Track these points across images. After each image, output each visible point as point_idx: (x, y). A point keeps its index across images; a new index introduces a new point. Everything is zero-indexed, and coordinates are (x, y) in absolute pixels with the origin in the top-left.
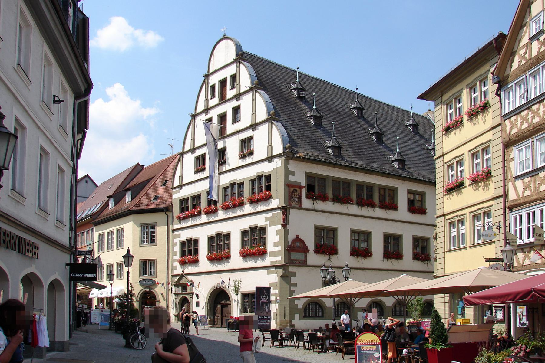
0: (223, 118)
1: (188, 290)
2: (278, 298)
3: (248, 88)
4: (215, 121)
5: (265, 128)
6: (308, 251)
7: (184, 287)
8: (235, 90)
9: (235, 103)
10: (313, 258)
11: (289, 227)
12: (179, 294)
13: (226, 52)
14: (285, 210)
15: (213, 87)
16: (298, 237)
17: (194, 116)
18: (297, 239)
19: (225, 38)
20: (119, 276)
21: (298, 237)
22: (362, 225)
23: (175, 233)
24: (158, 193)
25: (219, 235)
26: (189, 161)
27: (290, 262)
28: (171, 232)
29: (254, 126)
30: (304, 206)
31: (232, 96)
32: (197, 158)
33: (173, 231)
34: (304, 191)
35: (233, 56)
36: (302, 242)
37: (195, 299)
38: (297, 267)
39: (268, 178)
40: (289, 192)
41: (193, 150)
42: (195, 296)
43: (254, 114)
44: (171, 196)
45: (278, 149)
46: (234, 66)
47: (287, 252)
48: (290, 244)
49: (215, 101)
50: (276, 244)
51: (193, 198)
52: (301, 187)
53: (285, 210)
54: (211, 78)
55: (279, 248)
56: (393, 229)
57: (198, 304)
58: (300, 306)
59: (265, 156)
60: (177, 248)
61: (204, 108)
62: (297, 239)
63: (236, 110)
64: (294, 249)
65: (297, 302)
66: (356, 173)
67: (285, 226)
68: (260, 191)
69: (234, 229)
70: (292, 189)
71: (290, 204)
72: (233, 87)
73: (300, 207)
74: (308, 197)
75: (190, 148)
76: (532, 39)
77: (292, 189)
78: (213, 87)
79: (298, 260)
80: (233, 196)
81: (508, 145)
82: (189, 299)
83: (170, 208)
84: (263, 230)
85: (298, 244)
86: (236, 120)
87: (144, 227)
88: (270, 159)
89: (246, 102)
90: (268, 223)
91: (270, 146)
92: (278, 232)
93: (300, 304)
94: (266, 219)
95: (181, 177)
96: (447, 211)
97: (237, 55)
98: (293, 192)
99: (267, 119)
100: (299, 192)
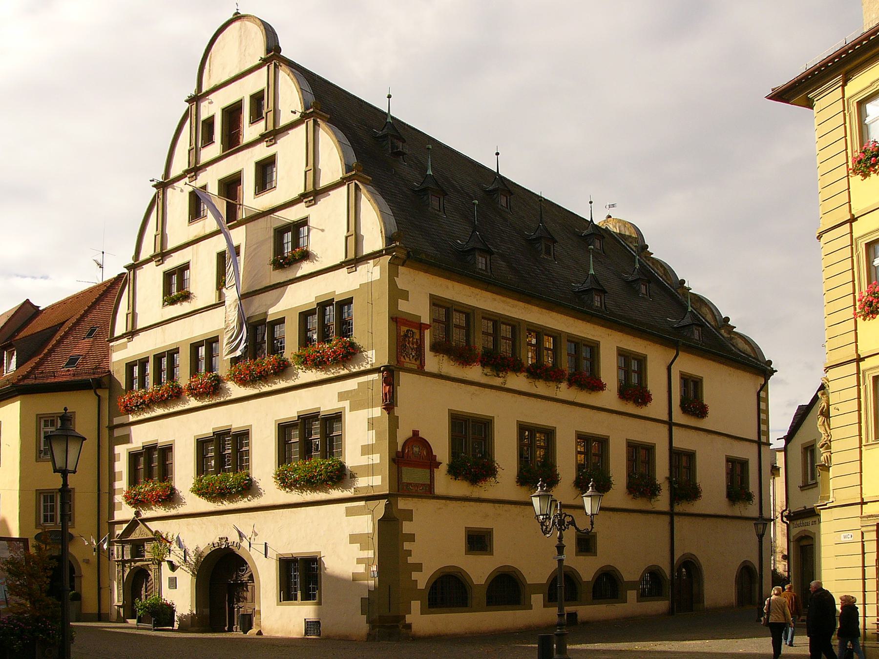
0: (230, 186)
2: (374, 568)
3: (297, 116)
7: (138, 548)
8: (263, 123)
9: (262, 152)
10: (443, 482)
11: (397, 411)
12: (128, 561)
13: (242, 49)
14: (390, 375)
15: (209, 123)
16: (416, 433)
17: (163, 186)
18: (416, 438)
19: (237, 17)
21: (416, 433)
22: (539, 414)
23: (118, 433)
24: (75, 352)
25: (220, 436)
26: (150, 281)
27: (399, 489)
28: (105, 432)
30: (427, 368)
31: (256, 136)
32: (168, 276)
33: (112, 428)
35: (259, 52)
36: (425, 444)
38: (415, 500)
40: (398, 335)
41: (162, 255)
44: (106, 356)
45: (373, 238)
47: (395, 467)
48: (400, 449)
50: (367, 450)
51: (158, 358)
52: (422, 327)
54: (204, 105)
55: (376, 458)
56: (596, 424)
57: (173, 583)
58: (422, 585)
59: (341, 258)
60: (122, 466)
61: (186, 167)
62: (416, 438)
63: (265, 170)
64: (408, 457)
65: (415, 575)
66: (527, 305)
67: (390, 405)
68: (324, 337)
70: (404, 329)
72: (257, 116)
73: (420, 371)
74: (436, 348)
75: (152, 253)
77: (404, 329)
78: (209, 123)
79: (417, 485)
83: (105, 380)
84: (336, 418)
85: (416, 449)
88: (354, 262)
90: (346, 404)
92: (372, 423)
93: (422, 579)
95: (133, 315)
97: (268, 51)
98: (406, 336)
99: (343, 179)
100: (417, 336)
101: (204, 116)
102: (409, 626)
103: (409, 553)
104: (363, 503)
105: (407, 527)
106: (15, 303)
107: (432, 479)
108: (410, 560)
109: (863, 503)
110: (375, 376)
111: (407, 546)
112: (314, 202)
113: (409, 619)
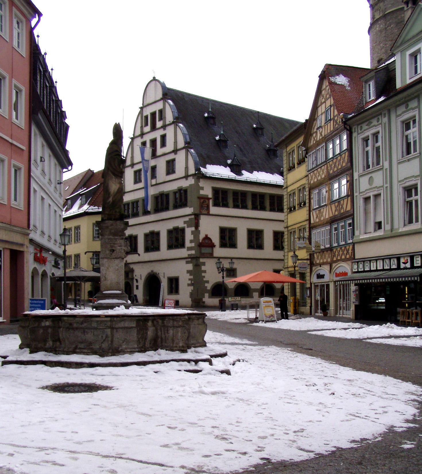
0: (153, 142)
1: (130, 276)
4: (148, 144)
5: (182, 153)
6: (215, 246)
10: (219, 251)
11: (200, 228)
15: (146, 117)
16: (206, 236)
18: (207, 238)
20: (77, 241)
21: (206, 236)
22: (256, 225)
29: (175, 151)
30: (211, 213)
32: (136, 172)
34: (211, 202)
35: (160, 95)
36: (210, 239)
37: (135, 284)
39: (186, 191)
40: (200, 203)
41: (132, 165)
42: (135, 281)
43: (176, 142)
46: (161, 103)
48: (201, 241)
49: (147, 129)
50: (191, 241)
52: (209, 199)
53: (197, 216)
55: (193, 245)
57: (137, 287)
62: (207, 238)
63: (163, 137)
65: (206, 285)
69: (163, 229)
70: (202, 200)
71: (200, 212)
73: (208, 214)
76: (318, 129)
77: (202, 200)
78: (146, 117)
79: (207, 253)
80: (162, 203)
81: (311, 189)
82: (131, 283)
84: (183, 230)
86: (163, 144)
87: (96, 255)
88: (186, 177)
89: (170, 132)
90: (186, 225)
91: (187, 168)
92: (193, 232)
93: (209, 286)
94: (185, 222)
96: (289, 224)
98: (203, 202)
101: (145, 114)
102: (204, 302)
103: (204, 277)
104: (190, 260)
105: (203, 268)
106: (87, 169)
107: (213, 251)
108: (204, 279)
109: (288, 268)
110: (193, 217)
111: (203, 274)
112: (176, 154)
113: (204, 300)
